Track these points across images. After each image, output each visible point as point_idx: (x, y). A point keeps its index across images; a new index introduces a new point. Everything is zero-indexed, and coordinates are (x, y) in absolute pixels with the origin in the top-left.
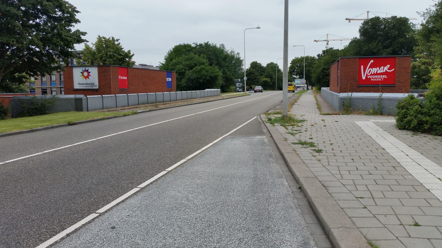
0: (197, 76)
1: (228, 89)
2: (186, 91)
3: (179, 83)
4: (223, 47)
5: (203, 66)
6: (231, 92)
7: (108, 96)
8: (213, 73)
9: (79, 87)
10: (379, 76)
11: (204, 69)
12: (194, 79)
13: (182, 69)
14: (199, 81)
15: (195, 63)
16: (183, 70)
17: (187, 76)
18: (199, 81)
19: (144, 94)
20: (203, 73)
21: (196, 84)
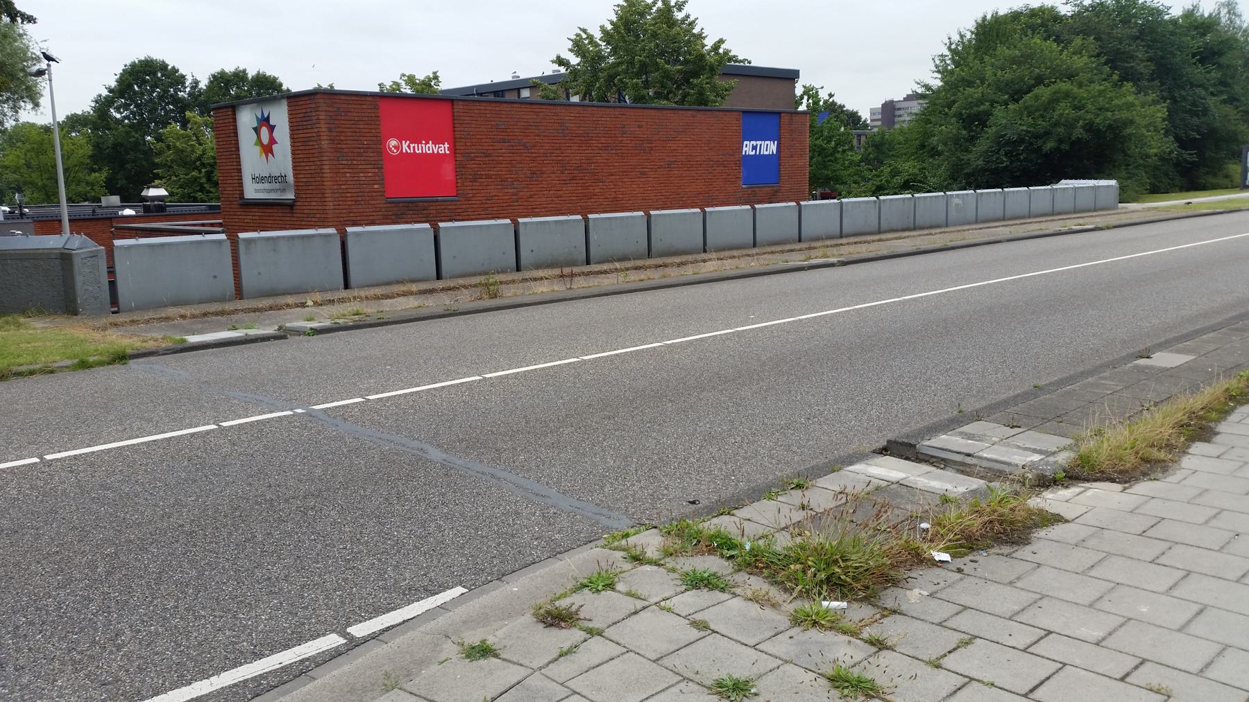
0: (1035, 125)
1: (1215, 175)
2: (1026, 188)
3: (962, 157)
4: (1229, 12)
5: (1064, 86)
6: (1227, 188)
7: (278, 238)
8: (1107, 110)
9: (257, 191)
10: (428, 152)
11: (1067, 95)
12: (1021, 141)
13: (980, 102)
14: (1040, 148)
15: (1039, 75)
16: (985, 106)
17: (994, 129)
18: (1040, 148)
19: (556, 222)
20: (1061, 115)
21: (1025, 159)
